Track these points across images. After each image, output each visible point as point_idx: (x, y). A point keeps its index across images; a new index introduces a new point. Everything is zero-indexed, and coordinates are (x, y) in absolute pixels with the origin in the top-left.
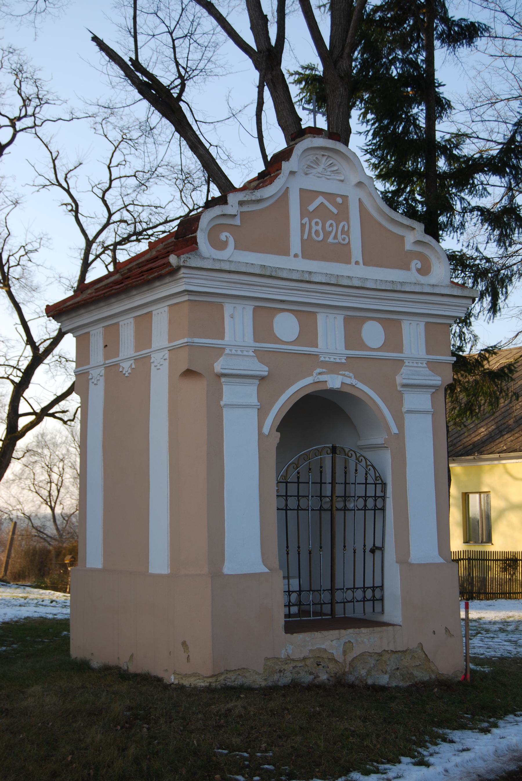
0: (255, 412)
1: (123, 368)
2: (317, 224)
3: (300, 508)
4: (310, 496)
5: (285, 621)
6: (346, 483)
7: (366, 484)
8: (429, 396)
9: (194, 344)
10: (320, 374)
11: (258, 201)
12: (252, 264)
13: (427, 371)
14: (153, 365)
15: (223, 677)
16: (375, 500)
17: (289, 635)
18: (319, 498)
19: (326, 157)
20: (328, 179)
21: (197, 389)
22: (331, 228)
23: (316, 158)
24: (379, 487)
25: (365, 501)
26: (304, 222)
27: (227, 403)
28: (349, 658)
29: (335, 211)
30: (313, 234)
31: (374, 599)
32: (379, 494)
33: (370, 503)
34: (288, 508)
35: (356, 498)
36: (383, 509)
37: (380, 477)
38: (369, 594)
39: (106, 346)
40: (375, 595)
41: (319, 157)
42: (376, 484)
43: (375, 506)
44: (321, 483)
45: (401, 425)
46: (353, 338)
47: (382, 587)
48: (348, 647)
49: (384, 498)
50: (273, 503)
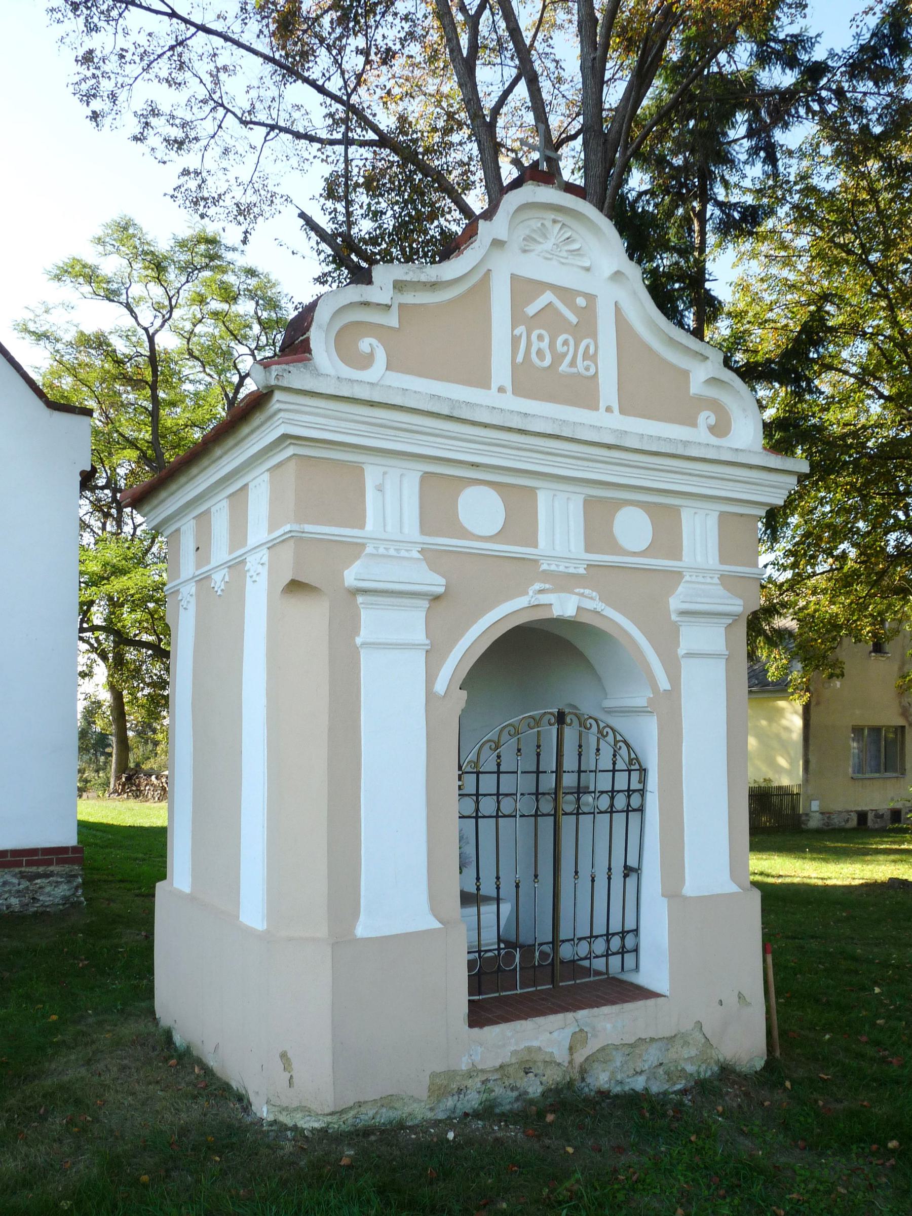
0: (421, 657)
1: (216, 582)
2: (540, 338)
3: (500, 814)
4: (518, 795)
5: (469, 1001)
6: (580, 771)
7: (614, 771)
8: (722, 630)
9: (304, 535)
10: (541, 591)
11: (434, 286)
12: (415, 392)
13: (720, 591)
14: (248, 574)
15: (352, 1113)
16: (629, 797)
17: (476, 1030)
18: (534, 797)
19: (559, 225)
20: (563, 264)
21: (312, 614)
22: (566, 348)
23: (542, 224)
24: (635, 776)
25: (612, 798)
26: (517, 332)
27: (368, 640)
28: (579, 1058)
29: (573, 319)
30: (534, 356)
31: (623, 951)
32: (635, 785)
33: (620, 802)
34: (480, 814)
35: (597, 795)
36: (641, 810)
37: (637, 759)
38: (616, 943)
39: (198, 548)
40: (626, 941)
41: (548, 224)
42: (629, 771)
43: (629, 805)
44: (538, 772)
45: (674, 676)
46: (598, 532)
47: (636, 931)
48: (578, 1039)
49: (642, 792)
50: (452, 806)
